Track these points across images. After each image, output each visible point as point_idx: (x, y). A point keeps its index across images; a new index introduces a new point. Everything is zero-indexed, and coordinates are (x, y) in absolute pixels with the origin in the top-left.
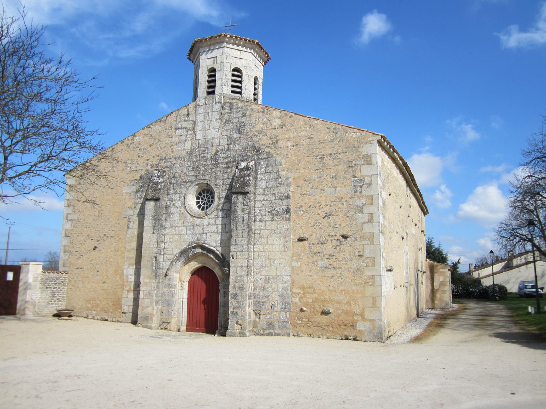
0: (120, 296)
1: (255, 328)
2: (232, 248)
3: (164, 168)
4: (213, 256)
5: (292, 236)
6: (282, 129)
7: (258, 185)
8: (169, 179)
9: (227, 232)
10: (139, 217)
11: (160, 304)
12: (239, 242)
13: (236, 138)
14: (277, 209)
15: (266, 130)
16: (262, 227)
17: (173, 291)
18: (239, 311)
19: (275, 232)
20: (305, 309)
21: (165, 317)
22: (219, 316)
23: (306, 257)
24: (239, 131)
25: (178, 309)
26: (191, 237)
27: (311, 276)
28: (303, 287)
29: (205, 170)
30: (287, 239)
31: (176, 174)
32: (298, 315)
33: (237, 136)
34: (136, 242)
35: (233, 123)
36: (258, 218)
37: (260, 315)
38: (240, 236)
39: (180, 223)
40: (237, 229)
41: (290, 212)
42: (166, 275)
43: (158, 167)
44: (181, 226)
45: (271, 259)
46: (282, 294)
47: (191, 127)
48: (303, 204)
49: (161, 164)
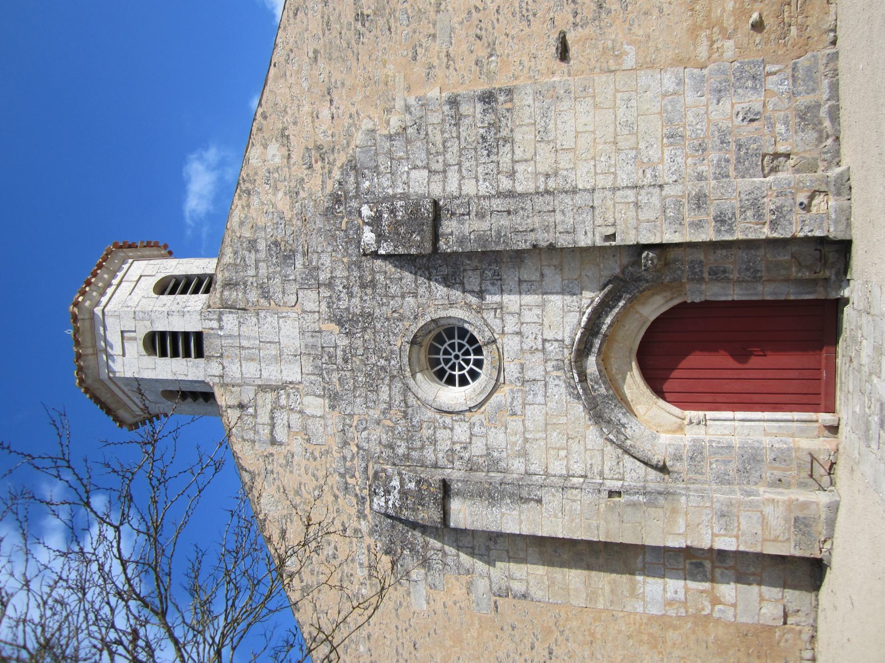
0: (732, 630)
1: (817, 166)
2: (584, 241)
3: (368, 479)
4: (607, 316)
5: (554, 79)
6: (291, 137)
7: (420, 192)
8: (397, 462)
9: (542, 275)
10: (495, 561)
11: (754, 488)
12: (567, 220)
13: (304, 265)
14: (482, 131)
15: (291, 181)
16: (530, 170)
17: (711, 446)
18: (769, 204)
19: (542, 129)
20: (755, 16)
21: (794, 473)
22: (783, 298)
23: (610, 30)
24: (289, 257)
25: (766, 434)
26: (556, 389)
27: (661, 11)
28: (693, 31)
29: (378, 351)
30: (562, 92)
31: (384, 442)
32: (773, 37)
33: (299, 261)
34: (566, 570)
35: (269, 274)
36: (505, 184)
37: (776, 156)
38: (552, 220)
39: (515, 424)
40: (532, 231)
41: (491, 92)
42: (663, 469)
43: (363, 498)
44: (523, 421)
45: (616, 135)
46: (715, 90)
47: (270, 397)
48: (474, 57)
49: (357, 488)
